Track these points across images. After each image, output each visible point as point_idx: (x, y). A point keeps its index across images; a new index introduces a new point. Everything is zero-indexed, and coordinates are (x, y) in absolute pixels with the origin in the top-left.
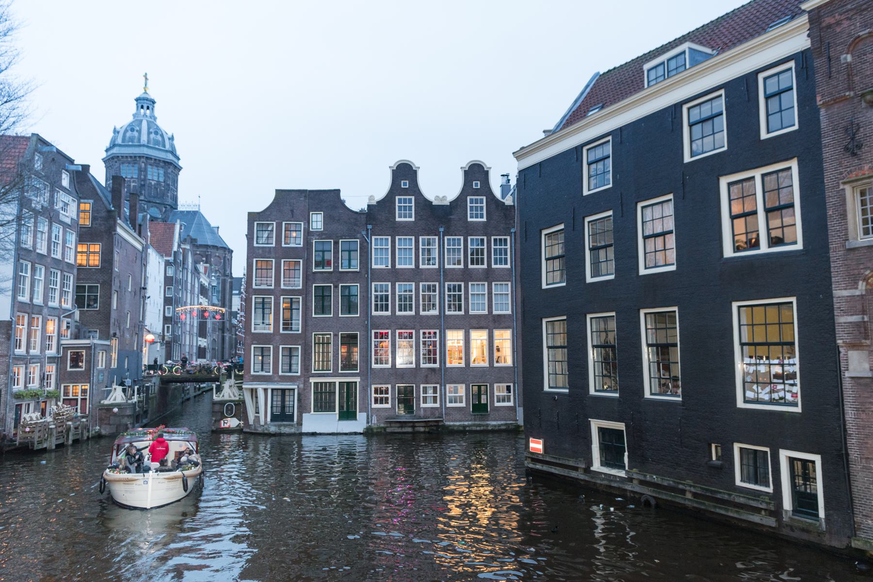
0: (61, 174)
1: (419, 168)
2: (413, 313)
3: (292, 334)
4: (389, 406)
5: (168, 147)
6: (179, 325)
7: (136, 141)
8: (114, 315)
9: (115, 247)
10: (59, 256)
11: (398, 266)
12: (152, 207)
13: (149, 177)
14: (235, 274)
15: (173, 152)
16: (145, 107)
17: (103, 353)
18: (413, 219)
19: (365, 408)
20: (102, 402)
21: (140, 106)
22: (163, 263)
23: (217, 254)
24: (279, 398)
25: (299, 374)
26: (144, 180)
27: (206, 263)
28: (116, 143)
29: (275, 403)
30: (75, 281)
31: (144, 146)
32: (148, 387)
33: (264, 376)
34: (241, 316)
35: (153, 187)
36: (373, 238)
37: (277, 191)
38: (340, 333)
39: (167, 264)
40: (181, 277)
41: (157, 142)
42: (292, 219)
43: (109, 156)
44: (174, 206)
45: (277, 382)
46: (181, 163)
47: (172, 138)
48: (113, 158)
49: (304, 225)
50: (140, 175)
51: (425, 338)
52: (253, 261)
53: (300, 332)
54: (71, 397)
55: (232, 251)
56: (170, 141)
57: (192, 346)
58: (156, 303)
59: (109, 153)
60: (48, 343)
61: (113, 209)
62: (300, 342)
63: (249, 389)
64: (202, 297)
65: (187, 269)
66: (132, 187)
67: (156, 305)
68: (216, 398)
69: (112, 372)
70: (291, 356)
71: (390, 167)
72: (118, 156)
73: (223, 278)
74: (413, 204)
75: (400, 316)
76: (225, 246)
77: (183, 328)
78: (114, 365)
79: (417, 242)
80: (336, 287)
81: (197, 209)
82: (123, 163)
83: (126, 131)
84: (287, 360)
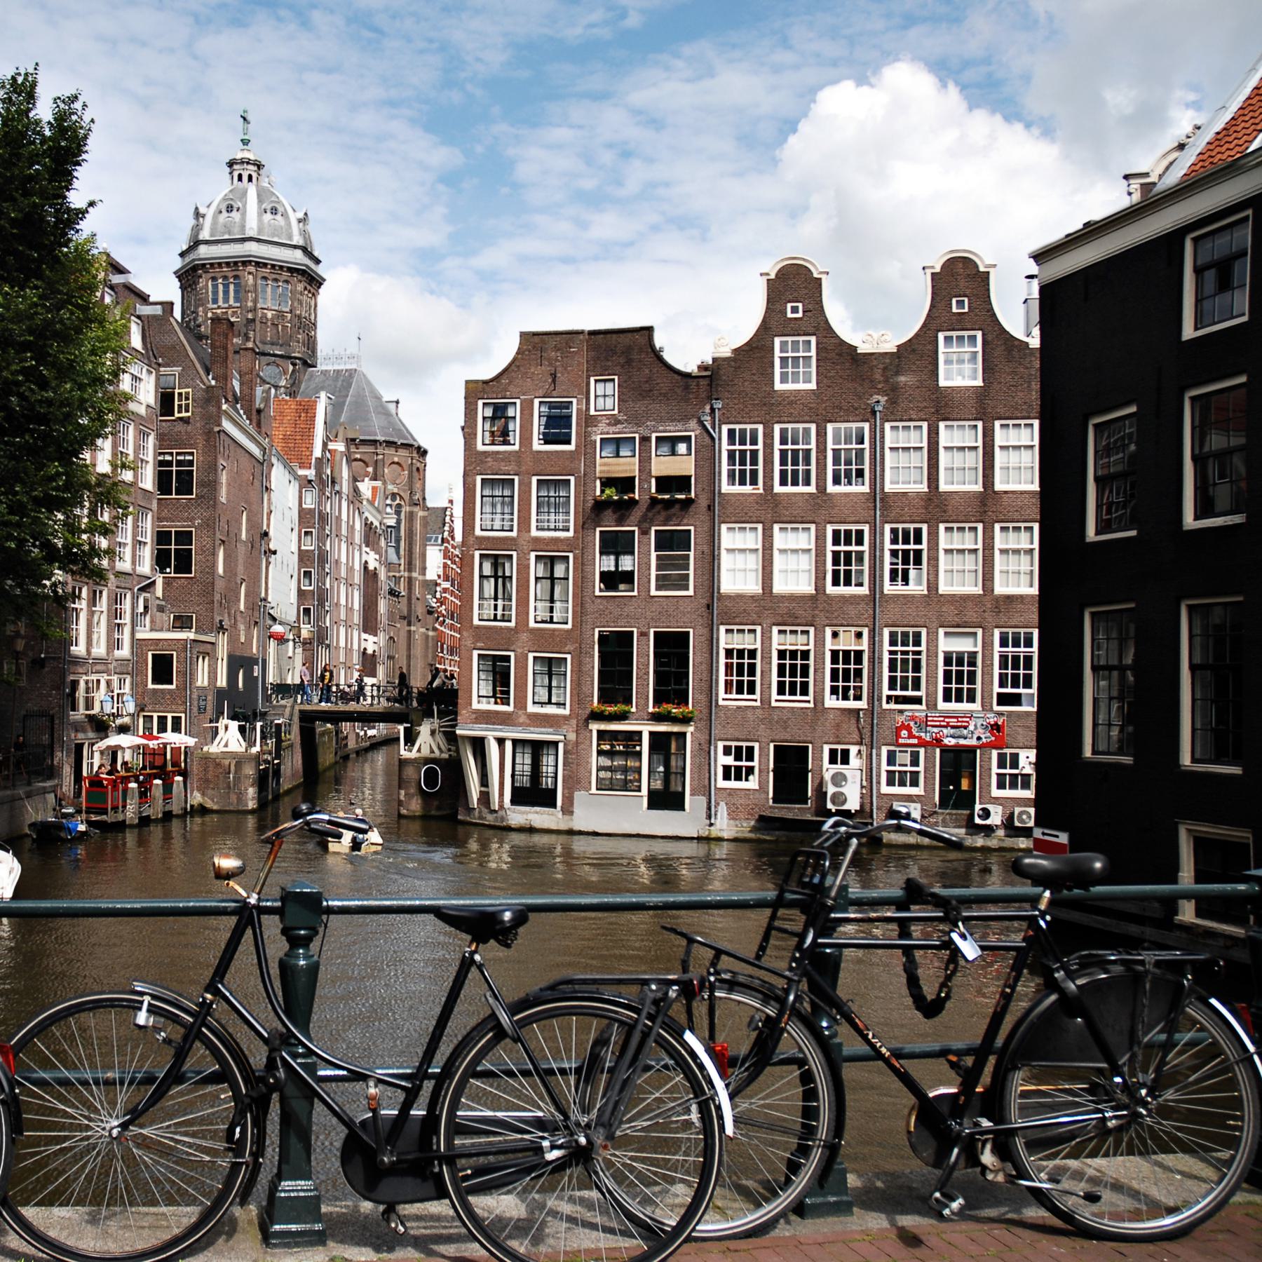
1: (828, 273)
3: (554, 630)
5: (297, 240)
6: (327, 608)
8: (220, 585)
9: (219, 456)
14: (435, 499)
16: (245, 178)
18: (813, 386)
19: (705, 789)
20: (205, 749)
23: (396, 459)
24: (528, 760)
26: (254, 310)
27: (375, 479)
28: (201, 237)
29: (518, 767)
31: (251, 239)
32: (279, 726)
34: (445, 590)
36: (725, 428)
40: (328, 510)
43: (188, 264)
44: (308, 363)
46: (321, 270)
49: (578, 404)
51: (915, 653)
52: (475, 481)
53: (569, 626)
55: (425, 452)
56: (301, 224)
57: (351, 649)
58: (285, 563)
59: (187, 260)
60: (116, 637)
61: (213, 383)
62: (569, 647)
64: (368, 550)
67: (285, 567)
68: (404, 753)
69: (221, 694)
71: (761, 275)
72: (204, 265)
73: (408, 509)
74: (813, 353)
76: (411, 442)
78: (222, 682)
80: (645, 532)
81: (354, 367)
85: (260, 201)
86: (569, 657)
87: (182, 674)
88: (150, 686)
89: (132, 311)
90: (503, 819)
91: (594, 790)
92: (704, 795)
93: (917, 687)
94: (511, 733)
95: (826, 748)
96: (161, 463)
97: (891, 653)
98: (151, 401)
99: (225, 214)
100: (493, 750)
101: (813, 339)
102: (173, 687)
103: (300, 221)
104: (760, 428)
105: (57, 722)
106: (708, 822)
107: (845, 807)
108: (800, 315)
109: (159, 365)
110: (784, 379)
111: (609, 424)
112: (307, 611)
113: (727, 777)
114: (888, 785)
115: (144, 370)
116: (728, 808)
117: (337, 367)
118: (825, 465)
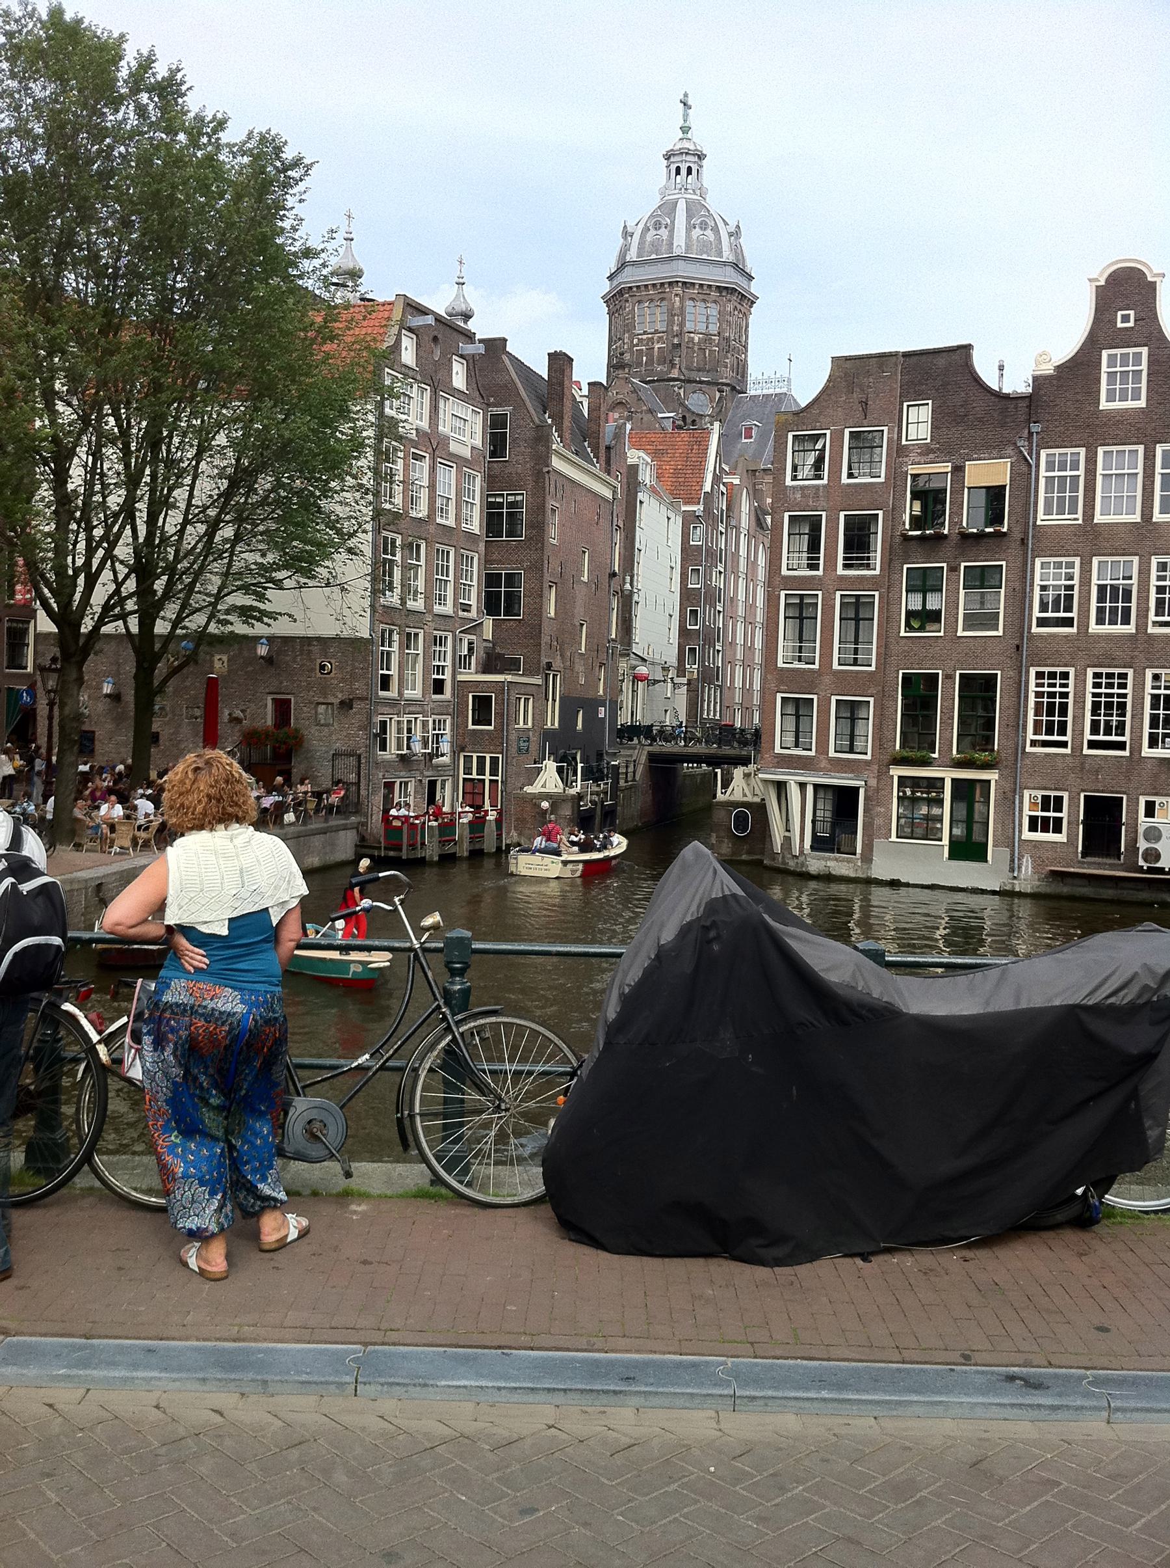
0: (450, 361)
1: (1164, 276)
2: (1131, 629)
3: (858, 672)
4: (1061, 838)
5: (727, 255)
7: (664, 248)
8: (547, 629)
9: (548, 497)
10: (451, 522)
11: (1098, 518)
12: (694, 392)
13: (689, 326)
15: (738, 267)
16: (684, 172)
17: (527, 700)
19: (1008, 840)
21: (673, 167)
22: (680, 520)
25: (868, 757)
26: (680, 334)
29: (819, 813)
30: (482, 567)
31: (679, 257)
33: (800, 757)
35: (696, 348)
37: (835, 360)
38: (958, 672)
39: (689, 520)
41: (705, 246)
42: (865, 422)
44: (737, 388)
45: (826, 772)
46: (754, 288)
47: (736, 234)
48: (621, 293)
50: (670, 323)
51: (1119, 696)
53: (873, 668)
54: (474, 776)
59: (615, 283)
62: (872, 691)
63: (773, 782)
65: (737, 528)
66: (656, 354)
69: (548, 735)
70: (853, 720)
71: (1090, 280)
74: (1144, 366)
75: (1099, 637)
77: (728, 653)
79: (1149, 458)
80: (954, 569)
81: (784, 390)
82: (639, 302)
83: (646, 229)
84: (791, 723)
85: (690, 216)
86: (871, 700)
87: (500, 715)
88: (471, 727)
89: (453, 350)
90: (803, 865)
91: (894, 838)
92: (1007, 847)
93: (1063, 732)
94: (812, 779)
95: (1142, 801)
96: (490, 505)
97: (1094, 695)
98: (478, 442)
99: (652, 232)
100: (794, 792)
101: (1145, 351)
102: (492, 728)
103: (731, 235)
104: (1082, 451)
105: (363, 761)
106: (1011, 875)
107: (1158, 865)
108: (1131, 324)
109: (488, 405)
110: (1111, 398)
111: (920, 454)
112: (692, 650)
113: (1033, 828)
114: (1030, 830)
115: (470, 411)
116: (1034, 861)
117: (765, 392)
118: (1153, 492)
